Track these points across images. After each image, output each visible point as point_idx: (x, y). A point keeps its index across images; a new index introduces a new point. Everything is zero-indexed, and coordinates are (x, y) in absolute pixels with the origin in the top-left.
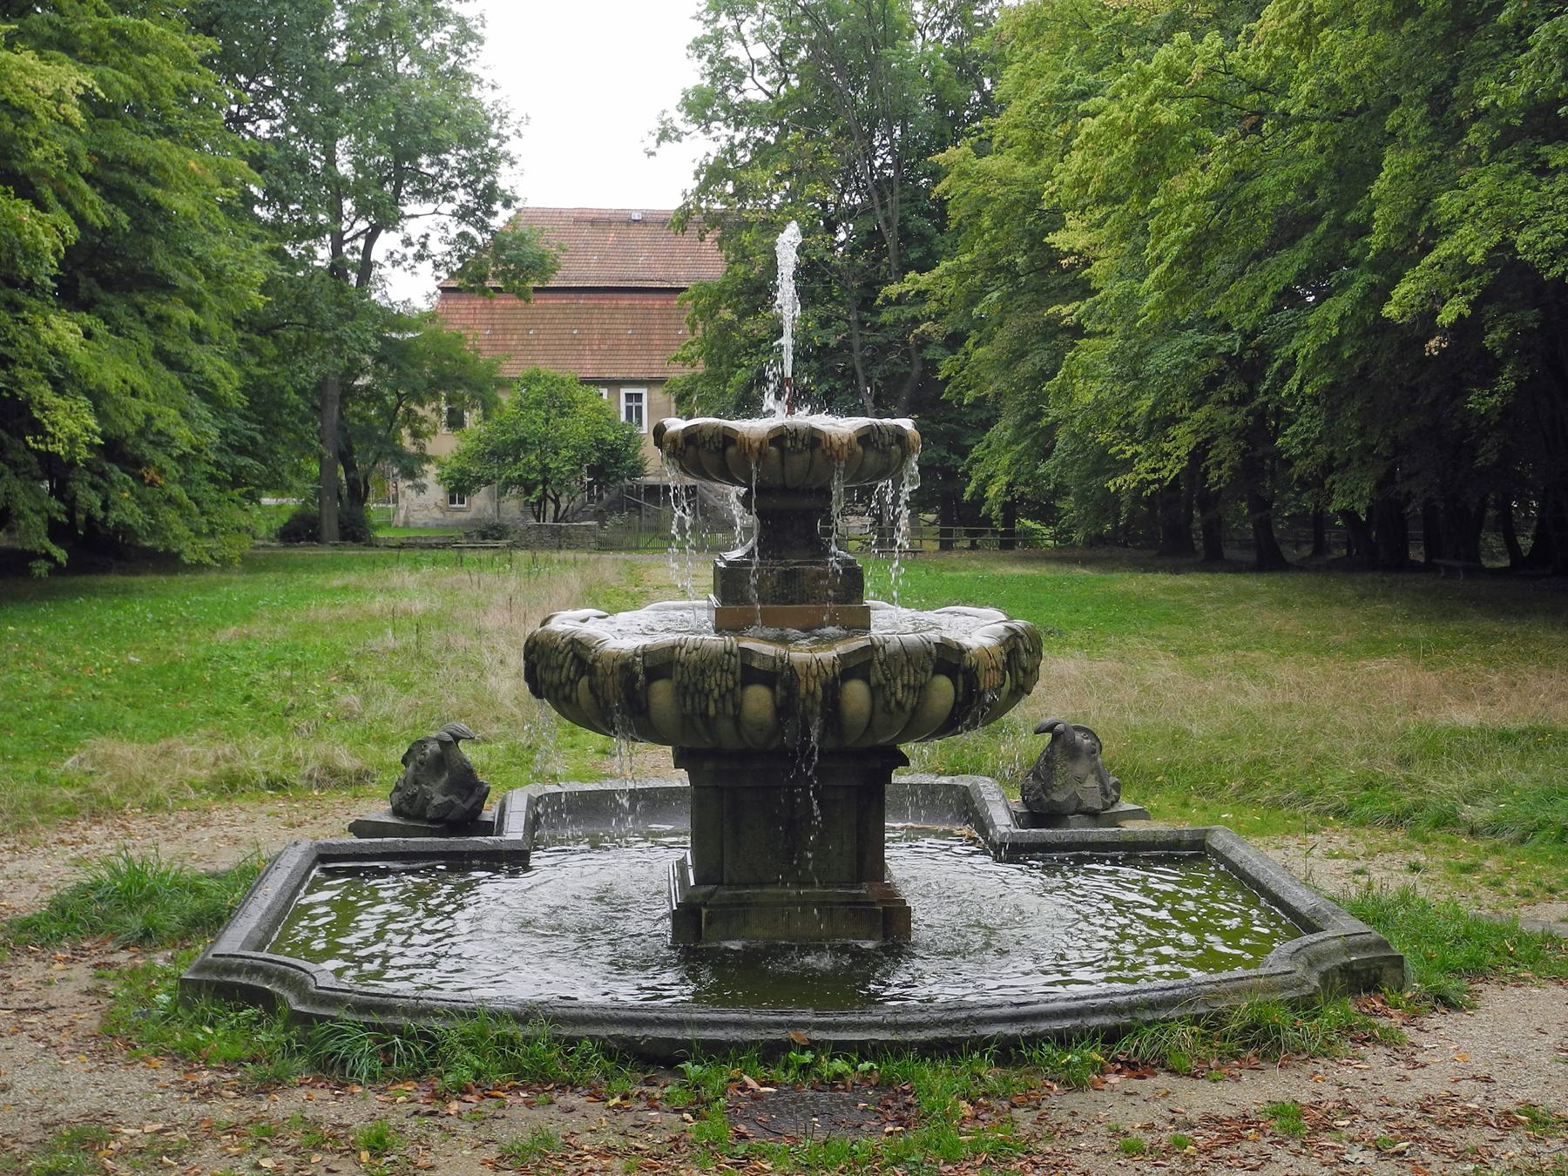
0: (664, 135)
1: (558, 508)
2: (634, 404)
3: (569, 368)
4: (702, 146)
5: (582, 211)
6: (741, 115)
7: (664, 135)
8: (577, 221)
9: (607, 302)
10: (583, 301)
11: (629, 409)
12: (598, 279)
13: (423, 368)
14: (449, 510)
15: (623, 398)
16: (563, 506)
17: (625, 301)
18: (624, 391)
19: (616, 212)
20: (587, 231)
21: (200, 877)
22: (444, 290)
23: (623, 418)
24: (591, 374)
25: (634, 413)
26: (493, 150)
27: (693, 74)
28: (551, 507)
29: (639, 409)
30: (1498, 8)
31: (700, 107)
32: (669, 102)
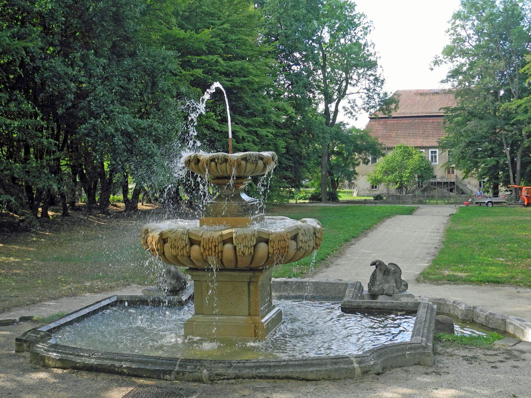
0: (436, 63)
1: (407, 189)
2: (434, 155)
3: (411, 143)
4: (448, 67)
5: (418, 91)
6: (464, 53)
7: (436, 63)
8: (415, 94)
9: (424, 120)
10: (417, 120)
11: (432, 156)
12: (422, 113)
13: (365, 146)
14: (371, 190)
15: (430, 153)
16: (409, 189)
17: (431, 120)
18: (430, 150)
19: (429, 90)
20: (419, 97)
21: (105, 218)
22: (371, 118)
23: (430, 159)
24: (419, 145)
25: (434, 158)
26: (70, 43)
27: (447, 41)
28: (404, 189)
29: (435, 156)
30: (234, 1)
31: (449, 52)
32: (439, 52)
